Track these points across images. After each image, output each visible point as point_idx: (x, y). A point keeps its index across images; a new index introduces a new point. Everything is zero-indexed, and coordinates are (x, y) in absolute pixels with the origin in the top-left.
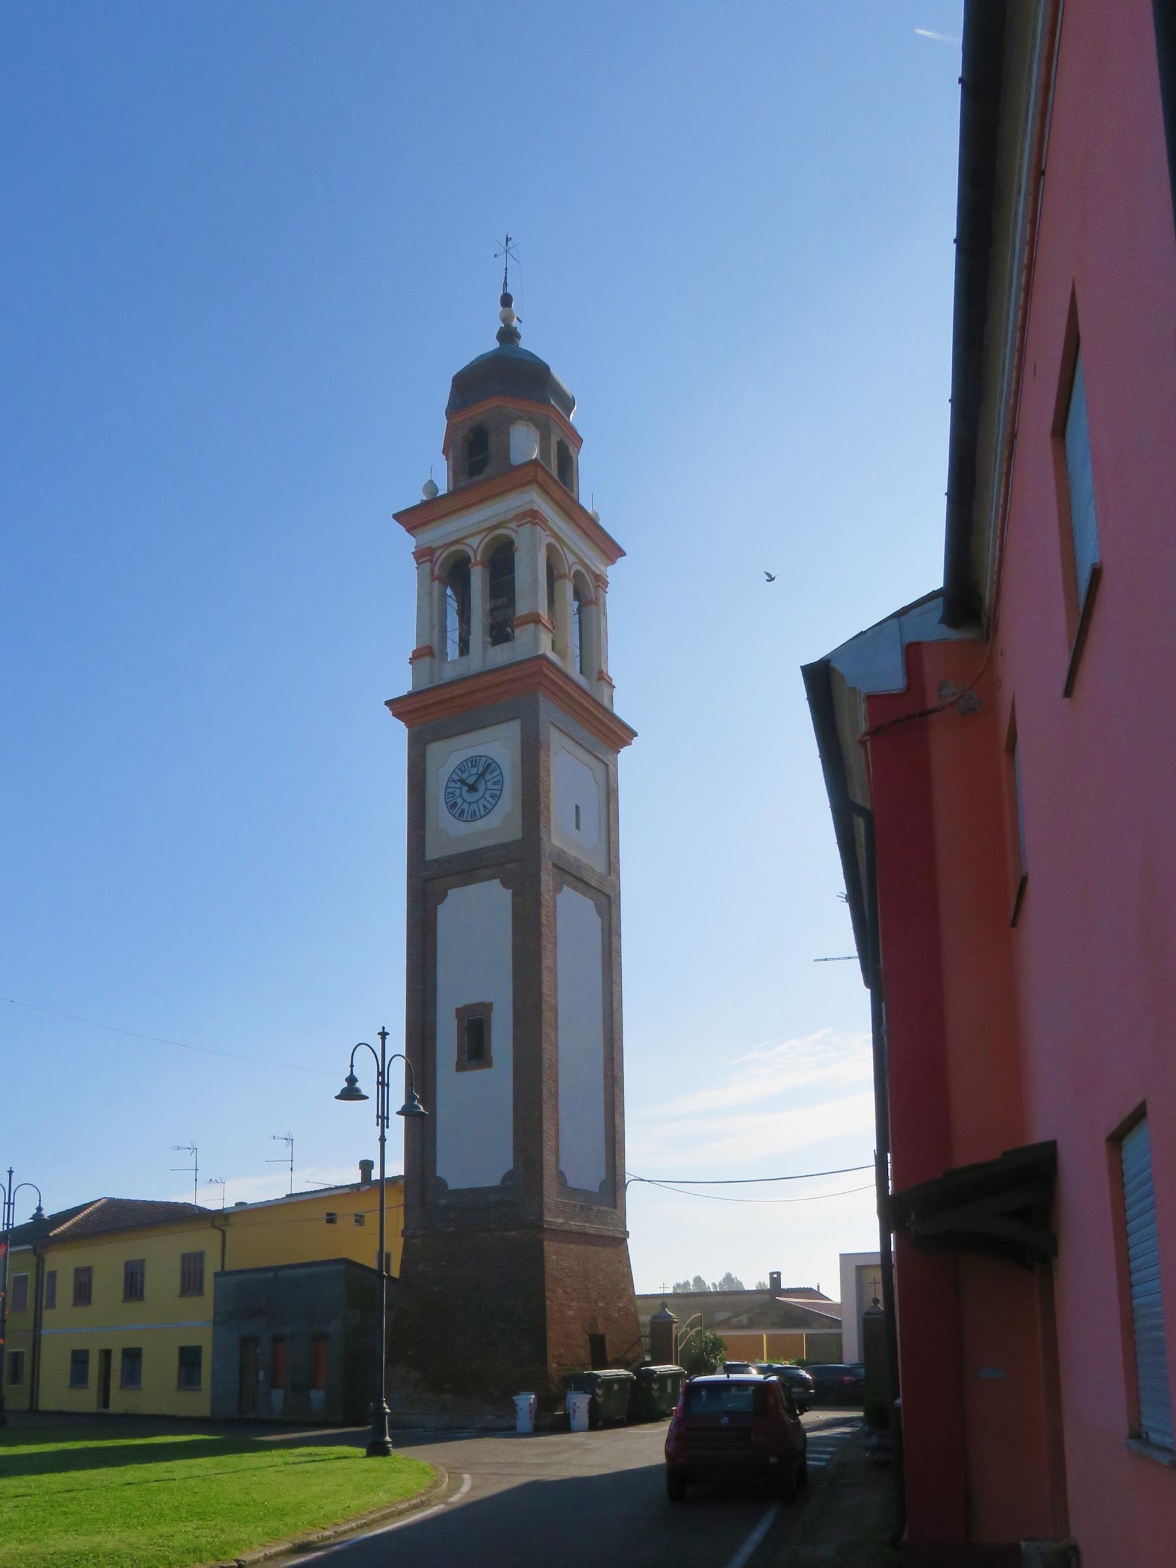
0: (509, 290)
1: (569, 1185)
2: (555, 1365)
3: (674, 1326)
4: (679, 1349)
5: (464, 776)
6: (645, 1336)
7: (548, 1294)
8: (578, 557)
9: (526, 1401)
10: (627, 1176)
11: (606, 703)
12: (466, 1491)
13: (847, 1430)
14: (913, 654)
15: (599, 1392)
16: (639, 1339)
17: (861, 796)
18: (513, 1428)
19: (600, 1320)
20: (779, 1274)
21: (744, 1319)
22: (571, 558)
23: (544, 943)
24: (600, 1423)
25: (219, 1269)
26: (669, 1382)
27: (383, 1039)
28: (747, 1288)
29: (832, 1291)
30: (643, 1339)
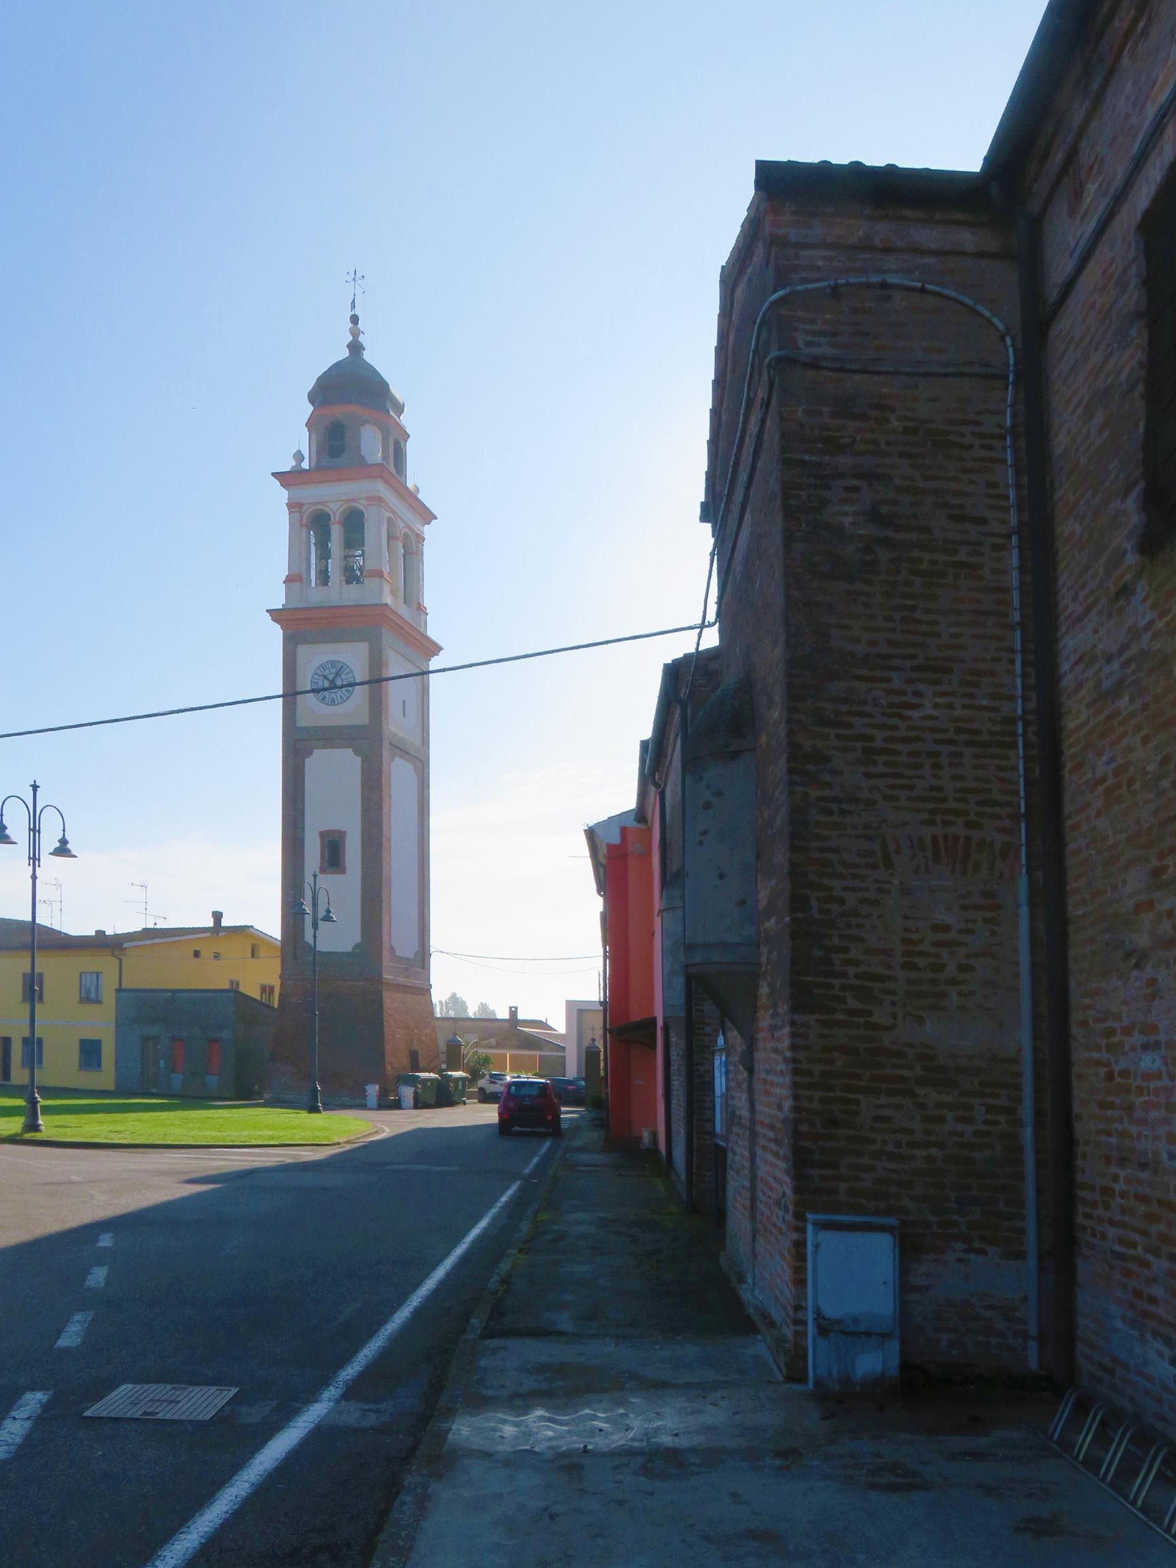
0: (357, 312)
1: (397, 954)
2: (389, 1068)
3: (462, 1047)
4: (465, 1062)
5: (326, 672)
6: (442, 1053)
7: (385, 1024)
8: (405, 523)
9: (373, 1090)
10: (431, 948)
11: (422, 630)
12: (386, 1133)
13: (575, 1116)
14: (624, 831)
15: (419, 1086)
16: (438, 1055)
17: (602, 860)
18: (365, 1106)
19: (415, 1041)
20: (516, 1008)
21: (493, 1041)
22: (401, 525)
23: (384, 796)
24: (420, 1105)
25: (117, 987)
26: (460, 1083)
27: (315, 878)
28: (499, 1017)
29: (559, 1024)
30: (441, 1055)
